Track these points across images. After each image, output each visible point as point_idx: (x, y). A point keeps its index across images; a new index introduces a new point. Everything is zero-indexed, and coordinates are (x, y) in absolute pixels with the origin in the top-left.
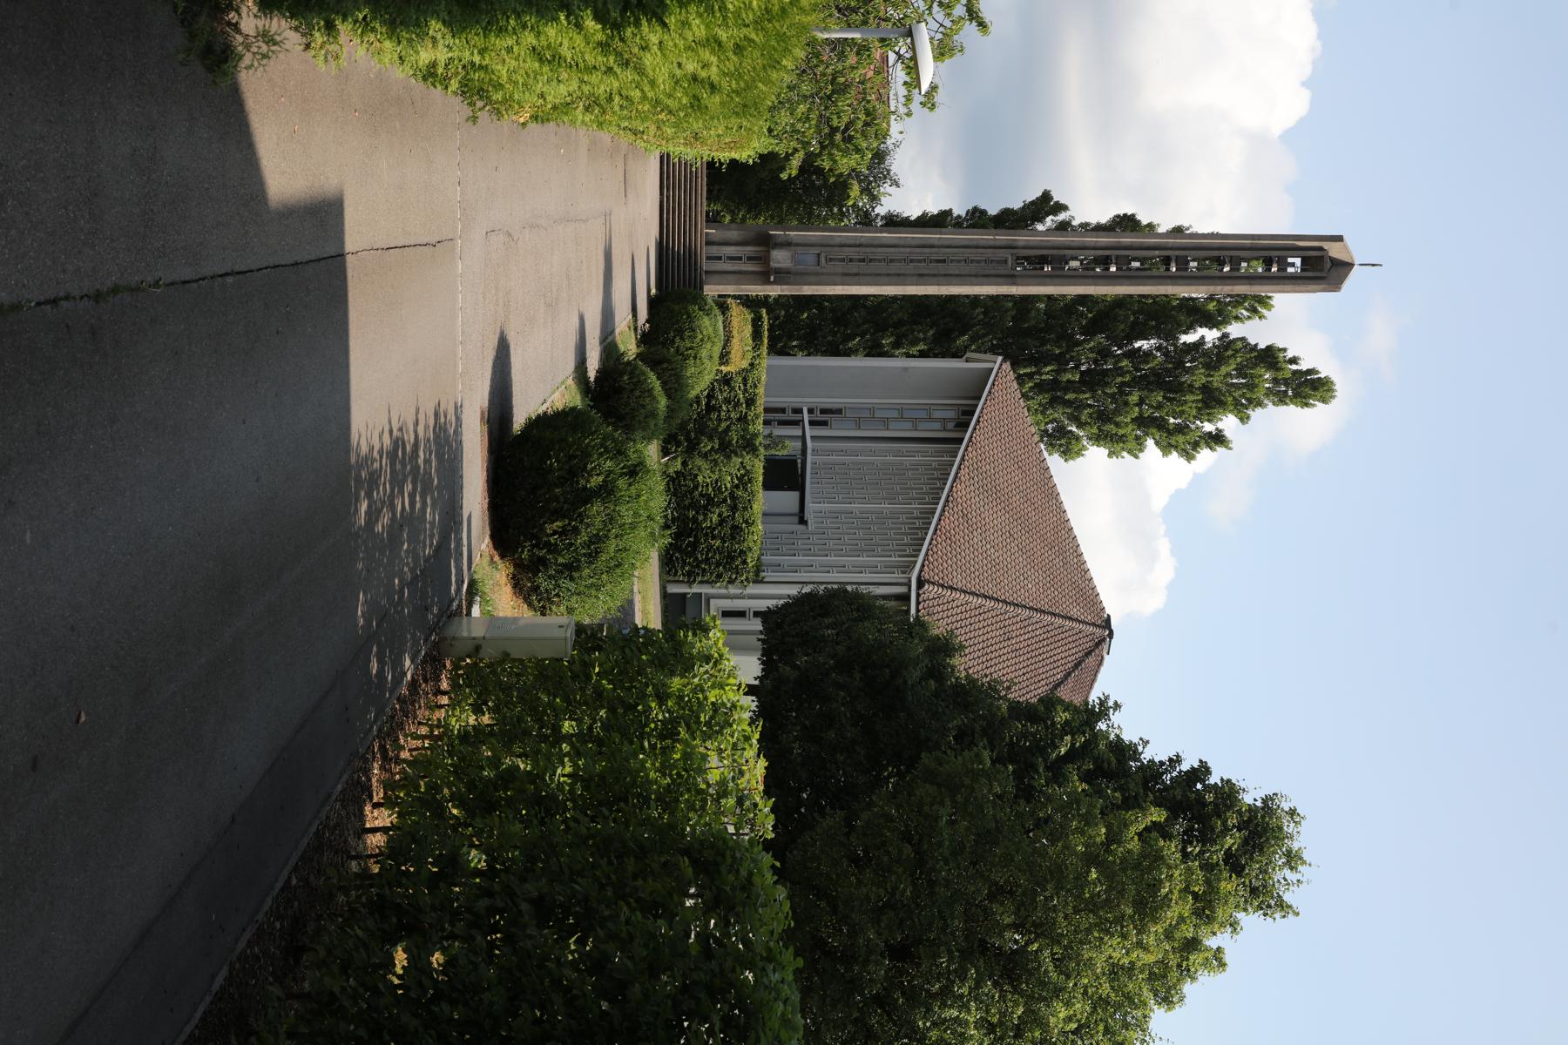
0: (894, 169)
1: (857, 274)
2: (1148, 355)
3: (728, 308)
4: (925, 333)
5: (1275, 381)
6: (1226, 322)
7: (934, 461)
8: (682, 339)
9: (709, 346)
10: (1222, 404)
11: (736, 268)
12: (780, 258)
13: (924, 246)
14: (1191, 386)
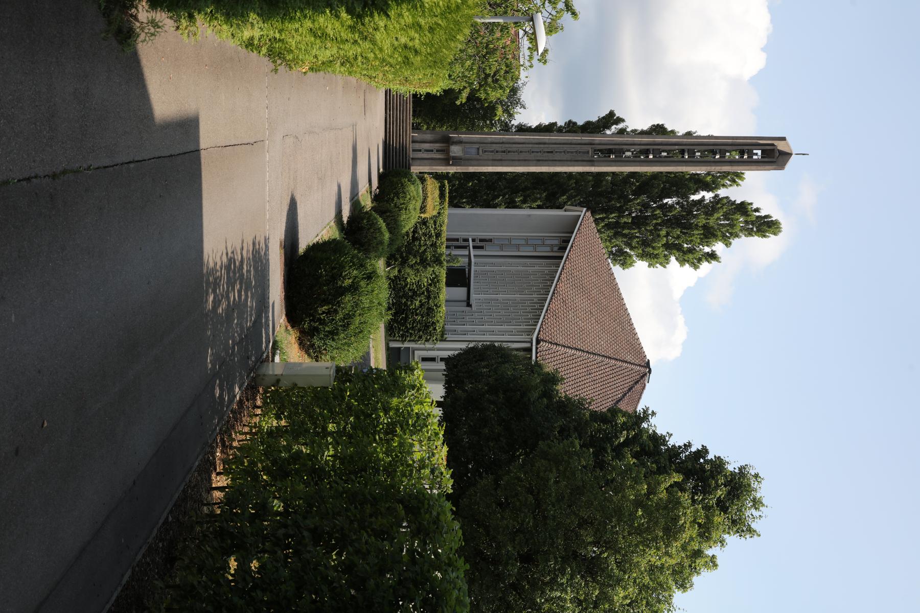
0: (523, 98)
4: (541, 194)
5: (746, 222)
6: (717, 187)
8: (398, 198)
10: (715, 236)
12: (456, 150)
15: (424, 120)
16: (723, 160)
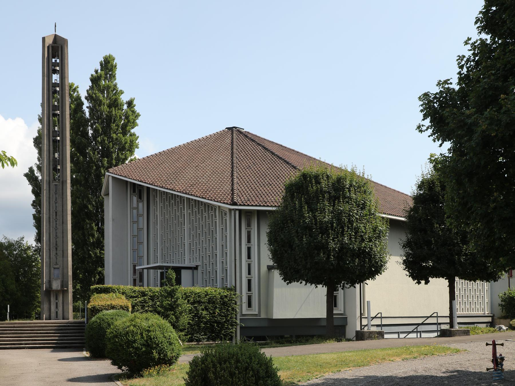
0: (16, 239)
1: (63, 251)
2: (95, 131)
3: (94, 307)
4: (87, 223)
5: (106, 78)
6: (79, 98)
8: (135, 341)
9: (138, 321)
10: (116, 100)
11: (61, 306)
12: (56, 285)
13: (50, 221)
14: (108, 112)
15: (33, 310)
16: (60, 85)
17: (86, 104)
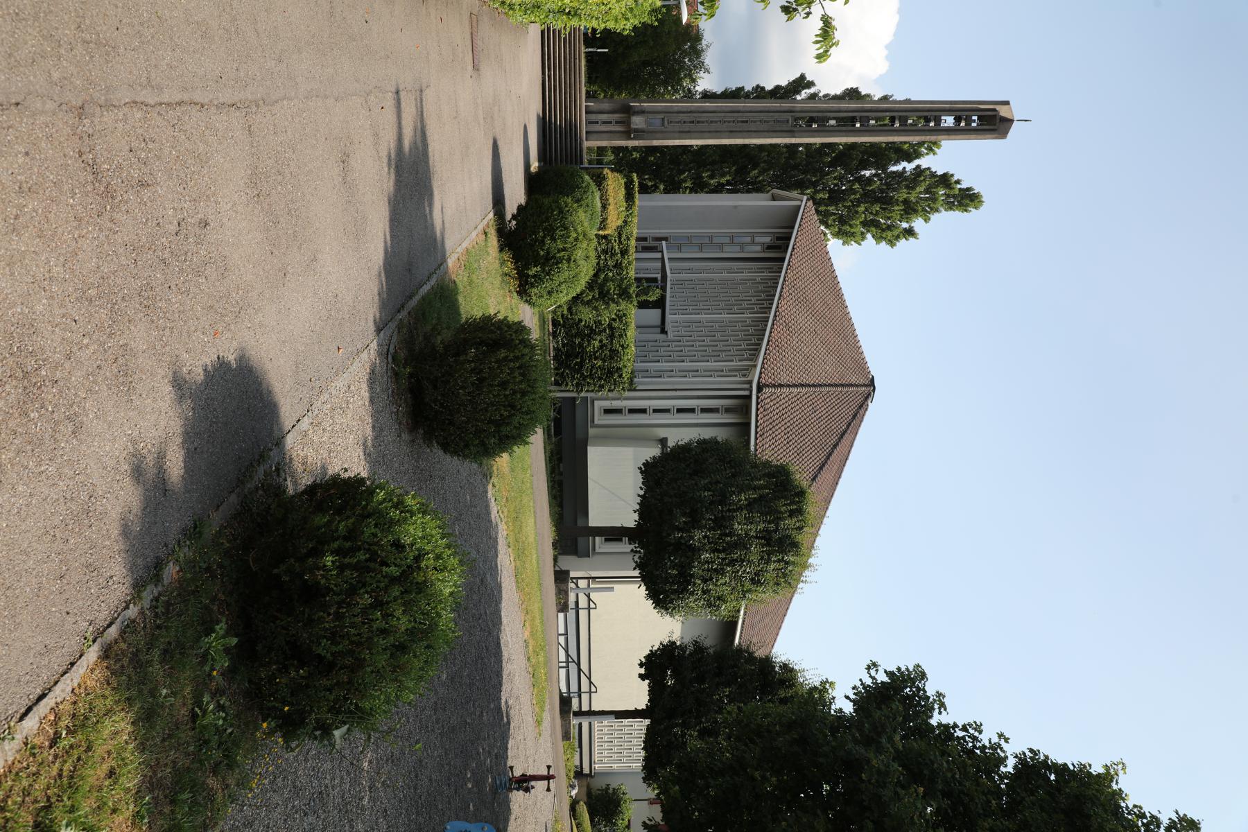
0: (707, 61)
2: (869, 181)
3: (604, 178)
5: (948, 196)
6: (918, 155)
7: (758, 276)
8: (553, 239)
9: (584, 245)
10: (915, 211)
17: (909, 167)
